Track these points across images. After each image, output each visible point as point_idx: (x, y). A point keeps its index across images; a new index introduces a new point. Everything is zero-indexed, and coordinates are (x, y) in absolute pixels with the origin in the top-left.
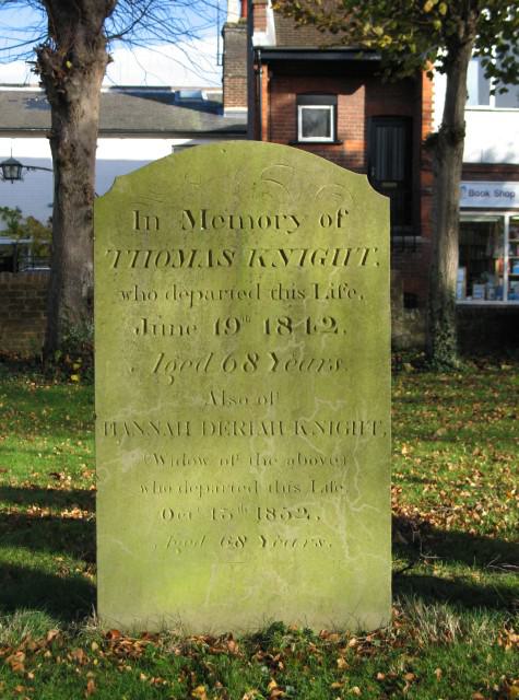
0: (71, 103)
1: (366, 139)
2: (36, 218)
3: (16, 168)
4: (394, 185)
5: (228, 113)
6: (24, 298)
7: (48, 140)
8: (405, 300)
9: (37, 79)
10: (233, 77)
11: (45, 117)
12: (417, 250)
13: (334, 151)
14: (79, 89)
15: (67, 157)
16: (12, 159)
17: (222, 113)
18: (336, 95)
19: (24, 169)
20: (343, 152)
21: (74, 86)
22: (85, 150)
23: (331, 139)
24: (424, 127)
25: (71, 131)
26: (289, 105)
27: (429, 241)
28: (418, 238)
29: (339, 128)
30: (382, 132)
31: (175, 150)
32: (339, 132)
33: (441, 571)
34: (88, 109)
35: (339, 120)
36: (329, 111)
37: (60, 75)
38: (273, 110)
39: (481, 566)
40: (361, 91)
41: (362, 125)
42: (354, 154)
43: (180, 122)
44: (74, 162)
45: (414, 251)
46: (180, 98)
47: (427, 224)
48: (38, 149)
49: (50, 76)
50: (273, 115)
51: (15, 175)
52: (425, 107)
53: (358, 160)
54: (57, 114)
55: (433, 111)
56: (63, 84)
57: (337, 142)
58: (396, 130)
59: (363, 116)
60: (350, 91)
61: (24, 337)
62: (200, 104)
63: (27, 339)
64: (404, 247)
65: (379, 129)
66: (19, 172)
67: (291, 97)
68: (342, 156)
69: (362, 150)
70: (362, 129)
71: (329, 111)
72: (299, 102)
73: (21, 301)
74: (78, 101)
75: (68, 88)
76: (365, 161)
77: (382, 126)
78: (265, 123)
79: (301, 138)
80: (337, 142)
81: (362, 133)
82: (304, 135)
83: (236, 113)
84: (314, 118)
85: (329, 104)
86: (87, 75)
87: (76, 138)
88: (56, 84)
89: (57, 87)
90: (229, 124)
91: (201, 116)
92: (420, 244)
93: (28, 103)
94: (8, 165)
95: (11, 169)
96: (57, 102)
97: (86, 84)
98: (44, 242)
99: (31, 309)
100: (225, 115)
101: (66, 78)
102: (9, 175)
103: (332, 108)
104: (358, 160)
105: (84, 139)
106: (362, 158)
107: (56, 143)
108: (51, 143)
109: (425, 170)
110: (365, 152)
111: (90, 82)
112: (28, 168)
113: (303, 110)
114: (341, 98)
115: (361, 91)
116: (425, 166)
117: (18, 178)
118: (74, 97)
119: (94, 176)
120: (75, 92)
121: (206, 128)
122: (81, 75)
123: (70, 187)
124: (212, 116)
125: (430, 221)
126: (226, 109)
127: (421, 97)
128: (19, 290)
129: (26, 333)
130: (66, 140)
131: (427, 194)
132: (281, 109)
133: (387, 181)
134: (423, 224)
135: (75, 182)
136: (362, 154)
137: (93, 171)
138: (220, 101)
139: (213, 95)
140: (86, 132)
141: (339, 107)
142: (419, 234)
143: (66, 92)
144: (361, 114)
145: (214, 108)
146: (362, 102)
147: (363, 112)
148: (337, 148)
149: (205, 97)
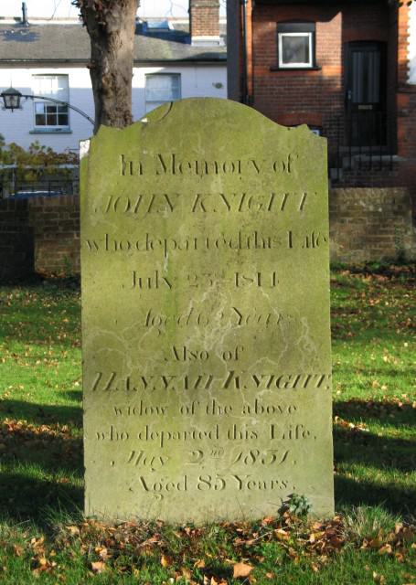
0: (111, 33)
1: (342, 64)
2: (18, 144)
3: (16, 98)
4: (371, 107)
5: (196, 42)
6: (58, 219)
7: (88, 70)
8: (413, 216)
9: (78, 11)
10: (200, 7)
11: (84, 48)
12: (394, 168)
13: (313, 77)
14: (118, 21)
15: (110, 85)
16: (11, 89)
17: (190, 42)
18: (314, 22)
19: (22, 99)
20: (320, 77)
21: (114, 18)
22: (124, 79)
23: (309, 65)
24: (400, 51)
25: (111, 61)
26: (270, 33)
27: (405, 160)
28: (395, 157)
29: (317, 54)
30: (358, 57)
31: (147, 78)
32: (317, 58)
33: (380, 477)
34: (125, 41)
35: (317, 46)
36: (307, 38)
37: (101, 8)
38: (256, 38)
39: (32, 482)
40: (339, 18)
41: (340, 50)
42: (332, 80)
43: (152, 51)
44: (115, 89)
45: (391, 169)
46: (148, 29)
47: (403, 143)
48: (81, 78)
49: (91, 9)
50: (255, 42)
51: (15, 104)
52: (401, 31)
53: (336, 85)
54: (96, 45)
55: (408, 35)
56: (104, 16)
57: (316, 67)
58: (371, 54)
59: (340, 42)
60: (328, 18)
61: (58, 256)
62: (167, 33)
63: (62, 258)
64: (381, 166)
65: (355, 54)
66: (18, 101)
67: (272, 25)
68: (320, 81)
69: (340, 74)
70: (340, 54)
71: (307, 38)
72: (280, 30)
73: (56, 223)
74: (118, 32)
75: (108, 20)
76: (342, 85)
77: (357, 51)
78: (249, 50)
79: (282, 65)
80: (316, 67)
81: (339, 58)
82: (285, 61)
83: (203, 42)
84: (293, 44)
85: (308, 32)
86: (124, 8)
87: (116, 67)
88: (97, 16)
89: (99, 19)
90: (198, 52)
91: (170, 45)
92: (396, 163)
93: (5, 35)
94: (7, 95)
95: (12, 98)
96: (96, 31)
97: (123, 16)
98: (28, 167)
99: (64, 230)
100: (193, 44)
101: (106, 11)
102: (8, 104)
103: (310, 35)
104: (336, 85)
105: (122, 68)
106: (339, 83)
107: (96, 73)
108: (91, 73)
109: (401, 92)
110: (343, 76)
111: (126, 14)
112: (27, 97)
113: (283, 37)
114: (319, 25)
115: (339, 18)
116: (401, 89)
117: (18, 107)
118: (114, 29)
119: (130, 103)
120: (115, 24)
121: (177, 57)
122: (119, 7)
123: (113, 113)
124: (181, 45)
125: (405, 141)
126: (193, 38)
127: (397, 22)
128: (53, 212)
129: (59, 253)
130: (107, 70)
131: (403, 115)
132: (263, 37)
133: (362, 104)
134: (399, 143)
135: (117, 109)
136: (339, 79)
137: (130, 98)
138: (187, 30)
139: (179, 25)
140: (123, 62)
141: (317, 33)
142: (396, 154)
143: (107, 24)
144: (338, 40)
145: (182, 37)
146: (340, 29)
147: (340, 37)
148: (315, 73)
149: (172, 28)
